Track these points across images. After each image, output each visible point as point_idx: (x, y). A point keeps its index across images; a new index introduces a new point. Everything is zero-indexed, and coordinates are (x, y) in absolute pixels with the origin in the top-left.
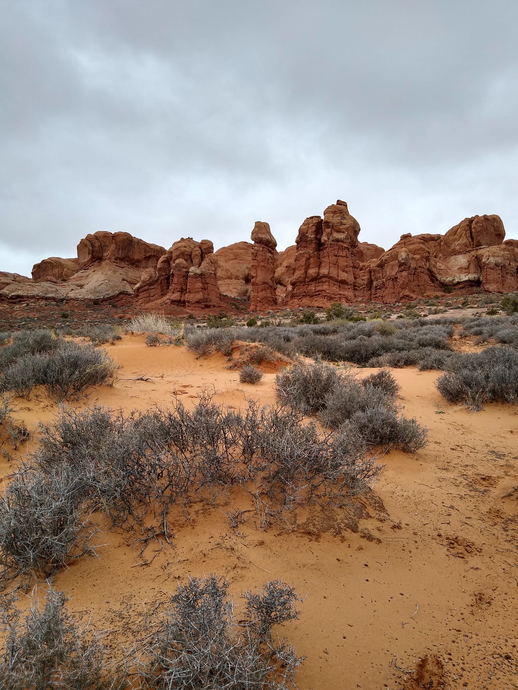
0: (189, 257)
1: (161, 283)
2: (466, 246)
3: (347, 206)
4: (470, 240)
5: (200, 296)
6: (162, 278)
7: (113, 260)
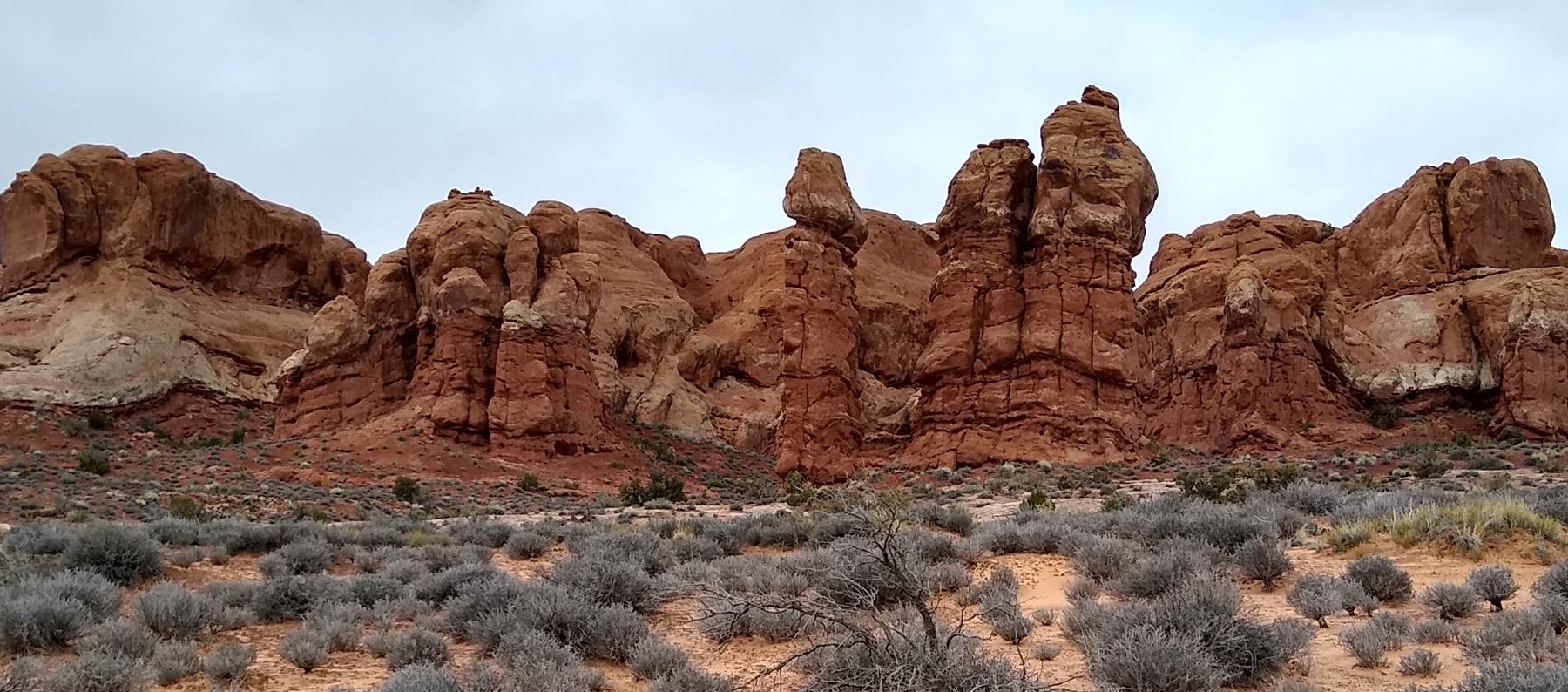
0: (495, 264)
1: (382, 357)
2: (1429, 266)
3: (1117, 109)
4: (1443, 246)
5: (541, 409)
6: (387, 336)
7: (140, 260)
